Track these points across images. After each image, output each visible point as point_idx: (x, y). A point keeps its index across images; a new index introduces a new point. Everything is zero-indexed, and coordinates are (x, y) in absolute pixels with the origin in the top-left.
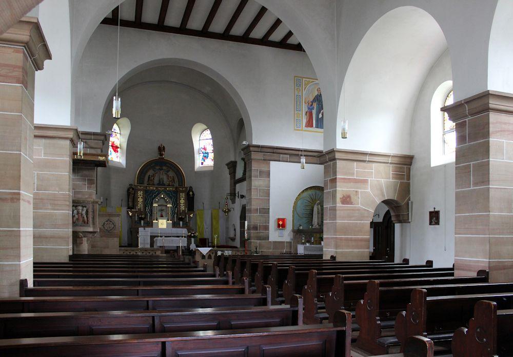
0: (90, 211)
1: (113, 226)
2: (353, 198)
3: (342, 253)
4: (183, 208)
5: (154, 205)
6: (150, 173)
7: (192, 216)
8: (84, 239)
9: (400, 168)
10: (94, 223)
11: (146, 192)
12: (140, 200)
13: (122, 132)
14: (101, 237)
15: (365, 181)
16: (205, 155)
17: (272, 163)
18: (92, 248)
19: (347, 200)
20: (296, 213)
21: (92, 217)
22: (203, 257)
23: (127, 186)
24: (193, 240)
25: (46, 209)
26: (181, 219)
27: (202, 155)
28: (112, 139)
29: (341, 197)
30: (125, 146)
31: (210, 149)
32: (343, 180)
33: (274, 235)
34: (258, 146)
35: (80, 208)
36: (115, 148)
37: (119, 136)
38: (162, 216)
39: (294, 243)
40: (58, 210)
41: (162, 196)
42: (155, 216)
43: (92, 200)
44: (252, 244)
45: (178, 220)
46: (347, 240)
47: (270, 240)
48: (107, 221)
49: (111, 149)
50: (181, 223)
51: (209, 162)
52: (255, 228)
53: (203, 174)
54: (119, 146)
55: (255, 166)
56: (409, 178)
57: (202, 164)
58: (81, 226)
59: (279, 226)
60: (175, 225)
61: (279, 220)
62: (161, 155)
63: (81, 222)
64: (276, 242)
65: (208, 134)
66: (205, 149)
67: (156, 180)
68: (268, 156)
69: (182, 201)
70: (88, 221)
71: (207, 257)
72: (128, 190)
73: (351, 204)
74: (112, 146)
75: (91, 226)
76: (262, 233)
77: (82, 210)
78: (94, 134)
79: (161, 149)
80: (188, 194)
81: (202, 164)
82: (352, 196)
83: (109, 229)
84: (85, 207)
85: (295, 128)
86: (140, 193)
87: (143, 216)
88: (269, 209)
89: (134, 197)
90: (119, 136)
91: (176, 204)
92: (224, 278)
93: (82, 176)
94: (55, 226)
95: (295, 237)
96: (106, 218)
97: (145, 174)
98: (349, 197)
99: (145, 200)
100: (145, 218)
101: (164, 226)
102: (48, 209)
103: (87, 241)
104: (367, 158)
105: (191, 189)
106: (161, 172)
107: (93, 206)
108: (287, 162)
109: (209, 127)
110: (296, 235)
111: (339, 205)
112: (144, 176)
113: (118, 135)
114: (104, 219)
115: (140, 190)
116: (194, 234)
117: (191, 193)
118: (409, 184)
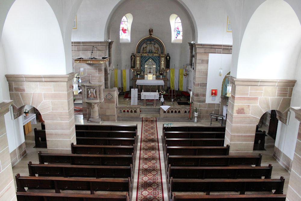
1: (111, 97)
2: (246, 110)
3: (234, 144)
4: (163, 66)
5: (145, 66)
6: (145, 45)
7: (168, 71)
8: (95, 105)
9: (285, 88)
10: (100, 98)
11: (141, 57)
12: (138, 62)
13: (128, 21)
14: (105, 103)
15: (256, 99)
16: (178, 32)
17: (210, 54)
18: (100, 109)
19: (241, 111)
20: (224, 85)
22: (165, 112)
24: (162, 96)
25: (57, 120)
26: (161, 74)
27: (176, 32)
28: (122, 26)
29: (237, 110)
30: (130, 29)
31: (181, 29)
32: (239, 99)
33: (209, 100)
34: (201, 45)
35: (92, 90)
36: (124, 31)
37: (127, 22)
38: (150, 73)
39: (221, 105)
40: (63, 120)
41: (150, 61)
42: (146, 73)
43: (98, 85)
44: (195, 105)
45: (160, 74)
46: (239, 136)
47: (206, 103)
49: (121, 32)
50: (161, 76)
51: (180, 37)
52: (197, 95)
53: (175, 45)
54: (126, 29)
55: (199, 57)
56: (290, 95)
57: (176, 38)
59: (212, 94)
60: (157, 78)
61: (212, 90)
62: (151, 35)
63: (92, 98)
64: (210, 104)
65: (179, 20)
66: (178, 29)
67: (148, 50)
68: (207, 50)
69: (163, 63)
71: (167, 112)
72: (131, 56)
73: (244, 113)
74: (123, 30)
75: (99, 99)
76: (202, 98)
78: (101, 42)
79: (151, 31)
80: (166, 58)
81: (176, 38)
82: (245, 109)
84: (95, 89)
85: (228, 31)
86: (138, 59)
87: (139, 73)
88: (206, 84)
89: (134, 61)
90: (127, 22)
91: (159, 65)
93: (95, 67)
94: (63, 129)
95: (222, 101)
97: (141, 47)
98: (243, 109)
99: (141, 62)
100: (140, 73)
101: (151, 79)
102: (59, 120)
103: (98, 106)
104: (259, 84)
105: (168, 55)
106: (151, 45)
107: (99, 88)
108: (215, 53)
109: (179, 16)
110: (223, 100)
111: (235, 114)
112: (141, 48)
113: (126, 22)
114: (107, 93)
115: (138, 57)
116: (163, 92)
117: (168, 58)
118: (290, 100)
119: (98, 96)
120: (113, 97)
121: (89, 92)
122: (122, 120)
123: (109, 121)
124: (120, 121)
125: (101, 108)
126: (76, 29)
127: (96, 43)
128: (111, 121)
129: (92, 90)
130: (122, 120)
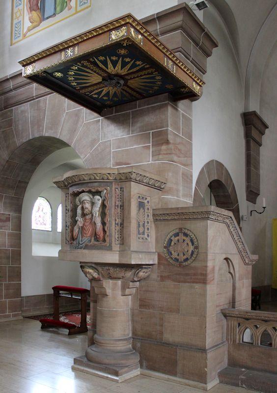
0: (112, 203)
1: (191, 248)
10: (123, 241)
14: (163, 278)
18: (141, 306)
21: (119, 221)
23: (241, 115)
35: (86, 197)
48: (177, 235)
58: (87, 247)
70: (104, 231)
75: (116, 247)
77: (93, 204)
83: (182, 258)
84: (98, 193)
92: (101, 121)
96: (173, 227)
103: (124, 287)
119: (113, 230)
120: (198, 249)
121: (79, 211)
122: (243, 382)
123: (174, 373)
124: (237, 385)
125: (143, 303)
126: (90, 6)
127: (166, 32)
128: (184, 375)
129: (86, 197)
130: (243, 382)
